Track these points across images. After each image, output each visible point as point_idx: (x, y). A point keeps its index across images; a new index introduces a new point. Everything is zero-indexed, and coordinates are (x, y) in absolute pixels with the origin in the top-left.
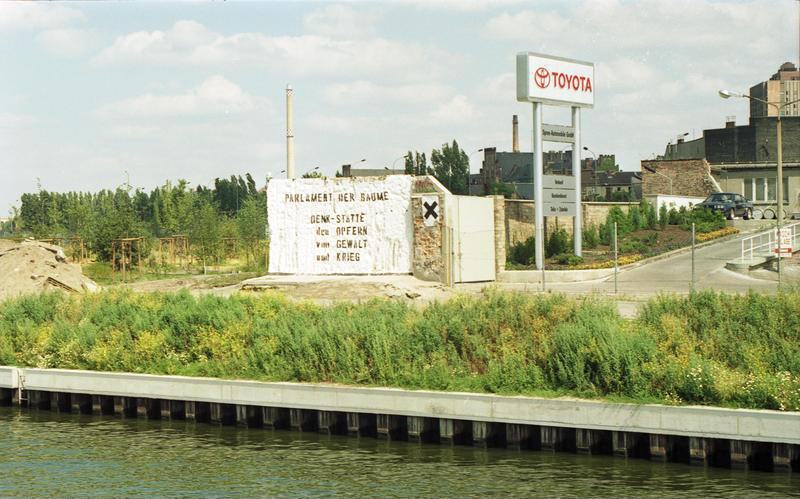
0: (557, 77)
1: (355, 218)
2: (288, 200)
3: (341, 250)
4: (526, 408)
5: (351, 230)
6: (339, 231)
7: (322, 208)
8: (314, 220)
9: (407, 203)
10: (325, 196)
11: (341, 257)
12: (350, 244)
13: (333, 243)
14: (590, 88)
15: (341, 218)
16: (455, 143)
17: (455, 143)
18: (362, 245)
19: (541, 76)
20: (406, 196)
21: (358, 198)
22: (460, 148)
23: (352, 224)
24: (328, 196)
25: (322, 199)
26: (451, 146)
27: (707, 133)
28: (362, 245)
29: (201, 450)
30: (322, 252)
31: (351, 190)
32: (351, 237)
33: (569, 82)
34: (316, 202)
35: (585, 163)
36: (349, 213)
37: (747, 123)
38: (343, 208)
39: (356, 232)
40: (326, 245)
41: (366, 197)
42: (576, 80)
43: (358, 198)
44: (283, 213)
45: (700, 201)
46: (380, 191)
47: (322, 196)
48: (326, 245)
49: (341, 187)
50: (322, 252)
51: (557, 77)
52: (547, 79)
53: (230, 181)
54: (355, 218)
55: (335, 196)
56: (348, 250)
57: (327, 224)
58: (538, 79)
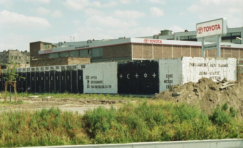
0: (205, 28)
2: (191, 65)
9: (235, 69)
14: (220, 28)
15: (211, 73)
19: (199, 30)
20: (234, 66)
21: (217, 66)
23: (215, 76)
24: (206, 65)
25: (204, 66)
29: (13, 105)
31: (214, 63)
33: (210, 29)
34: (201, 67)
35: (32, 63)
36: (214, 71)
37: (39, 54)
38: (212, 69)
41: (220, 65)
42: (207, 28)
43: (217, 66)
44: (189, 70)
46: (225, 63)
47: (204, 64)
49: (211, 61)
51: (205, 28)
52: (202, 31)
55: (209, 65)
58: (198, 31)
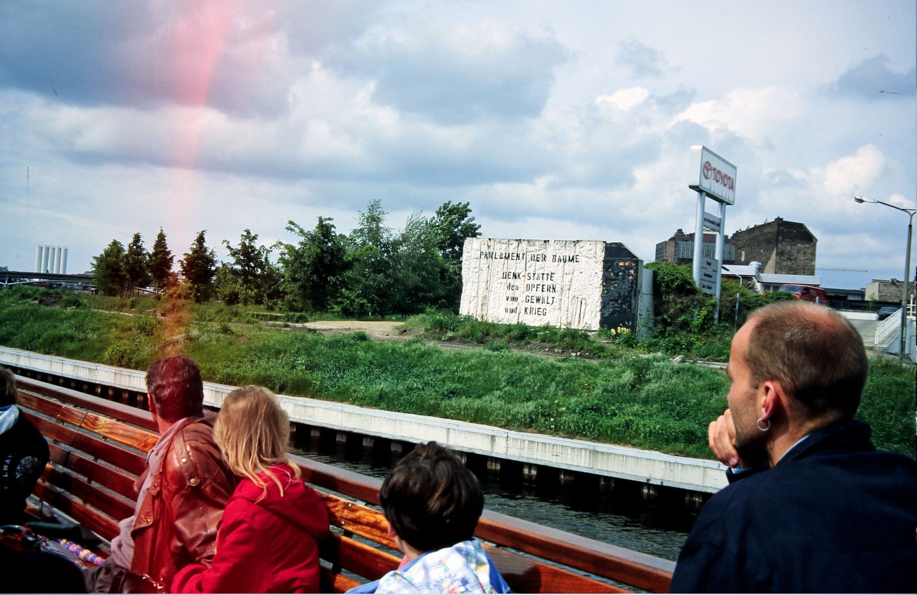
1: (545, 276)
3: (529, 305)
4: (644, 313)
5: (540, 287)
6: (528, 287)
7: (514, 266)
8: (506, 276)
10: (518, 256)
11: (528, 311)
12: (538, 300)
13: (522, 298)
16: (480, 234)
17: (480, 234)
18: (550, 301)
21: (549, 258)
22: (98, 256)
24: (521, 256)
26: (149, 247)
27: (779, 221)
28: (550, 301)
30: (513, 305)
32: (539, 294)
38: (533, 266)
39: (545, 289)
40: (514, 299)
45: (774, 256)
48: (514, 299)
50: (513, 305)
53: (172, 271)
54: (545, 276)
56: (536, 305)
57: (518, 280)
